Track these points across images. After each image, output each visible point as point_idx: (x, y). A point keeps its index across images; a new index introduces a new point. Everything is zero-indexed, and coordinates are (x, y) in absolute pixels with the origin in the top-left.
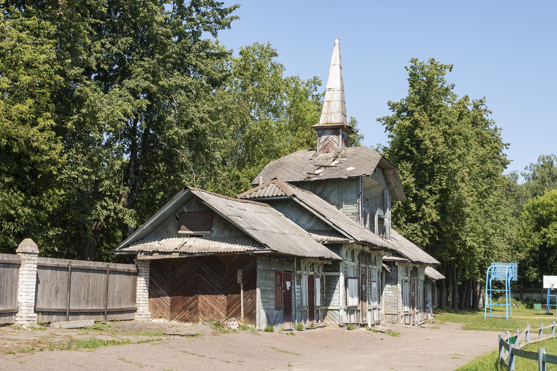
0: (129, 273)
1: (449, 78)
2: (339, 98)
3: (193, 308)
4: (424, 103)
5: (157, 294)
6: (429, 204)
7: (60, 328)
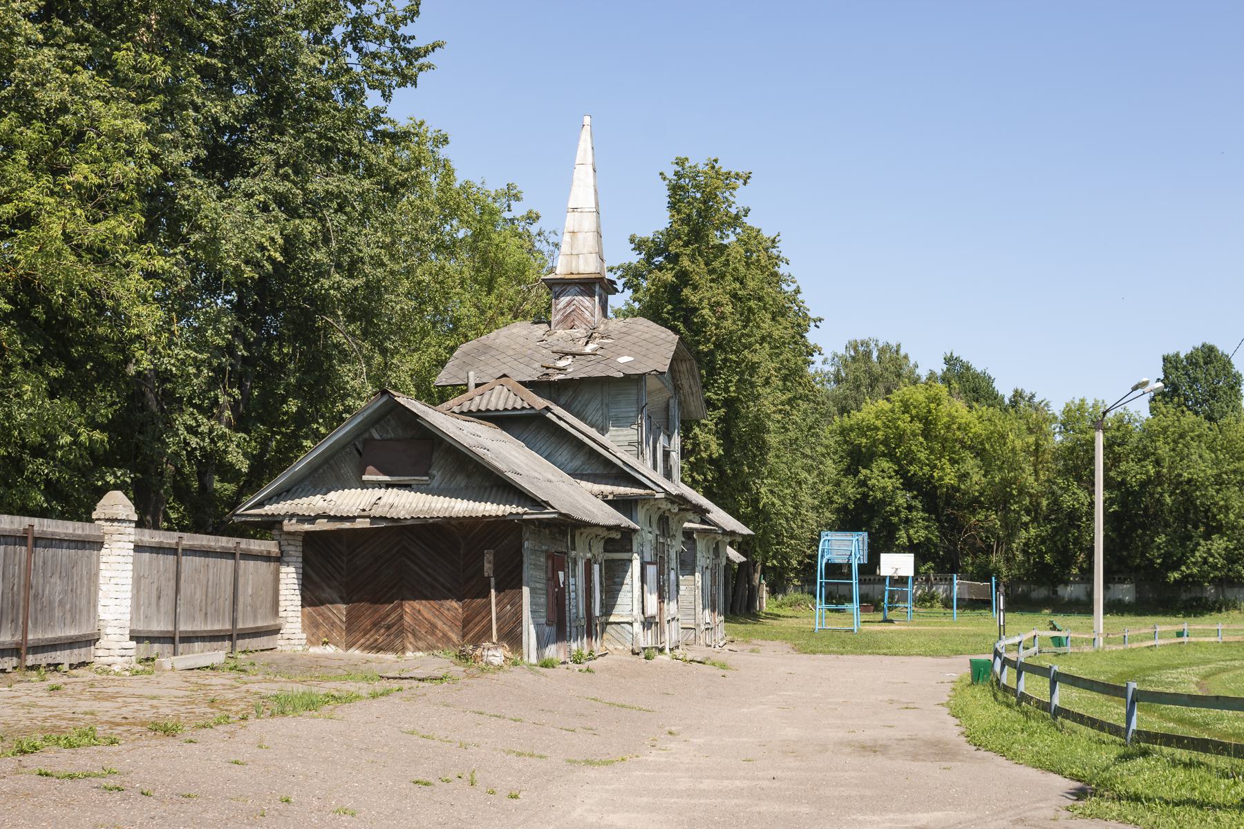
0: (267, 558)
1: (740, 198)
2: (594, 227)
3: (394, 624)
4: (696, 241)
5: (319, 599)
6: (706, 425)
7: (173, 669)
